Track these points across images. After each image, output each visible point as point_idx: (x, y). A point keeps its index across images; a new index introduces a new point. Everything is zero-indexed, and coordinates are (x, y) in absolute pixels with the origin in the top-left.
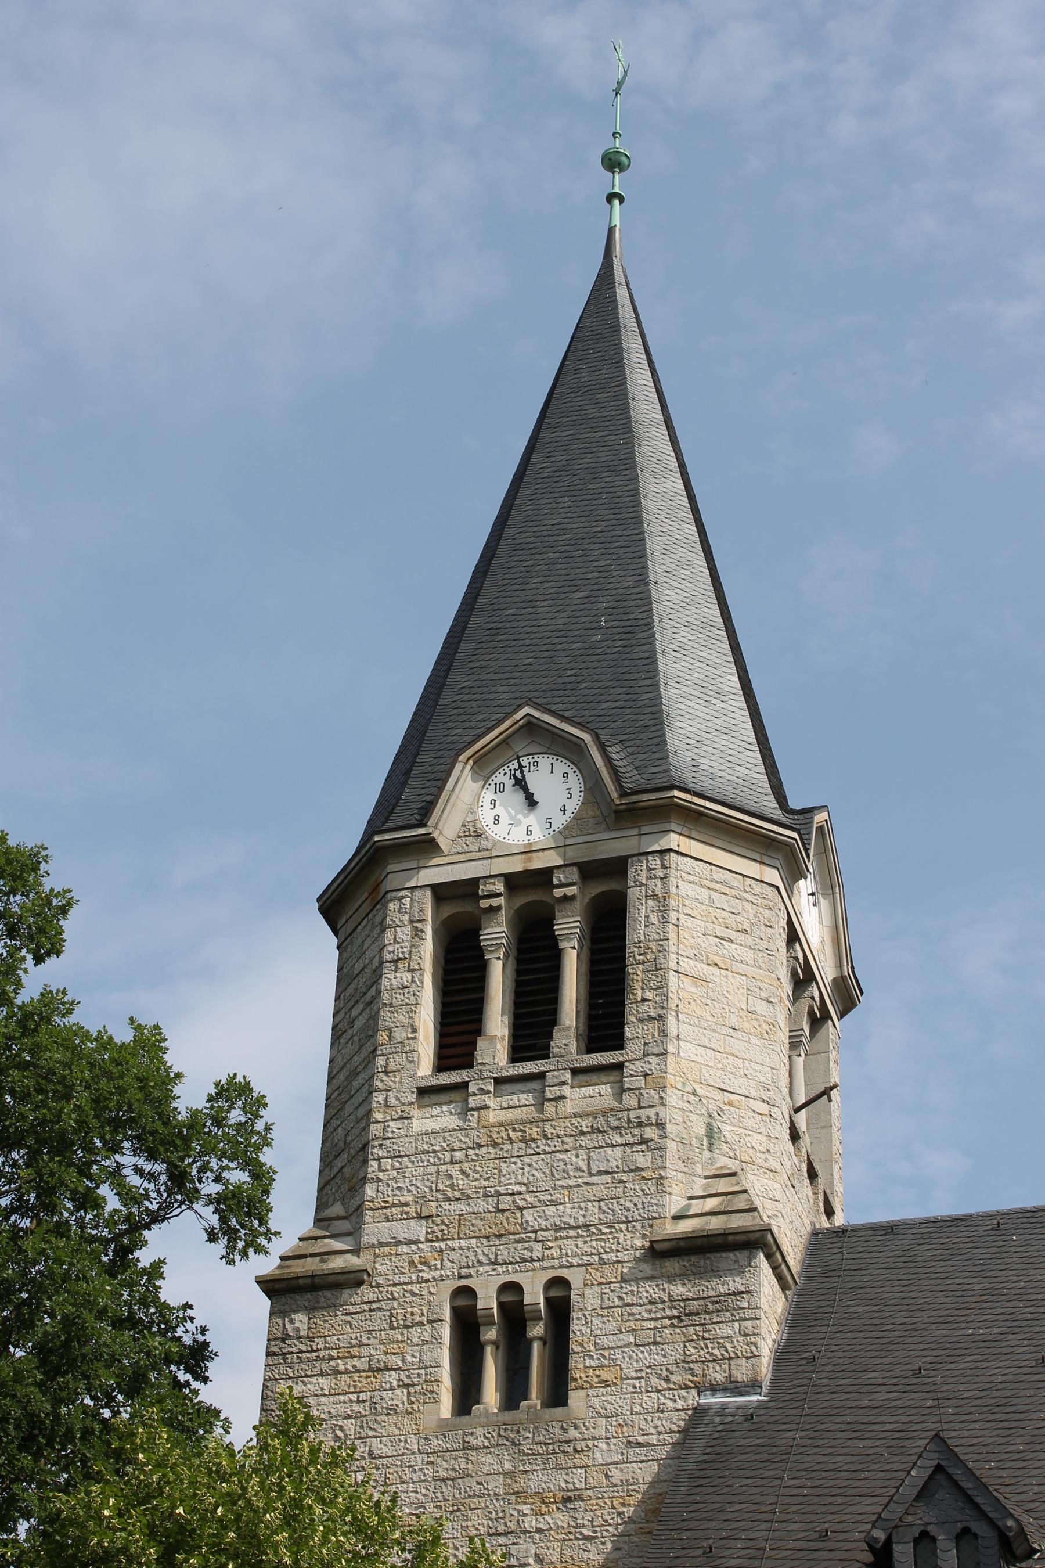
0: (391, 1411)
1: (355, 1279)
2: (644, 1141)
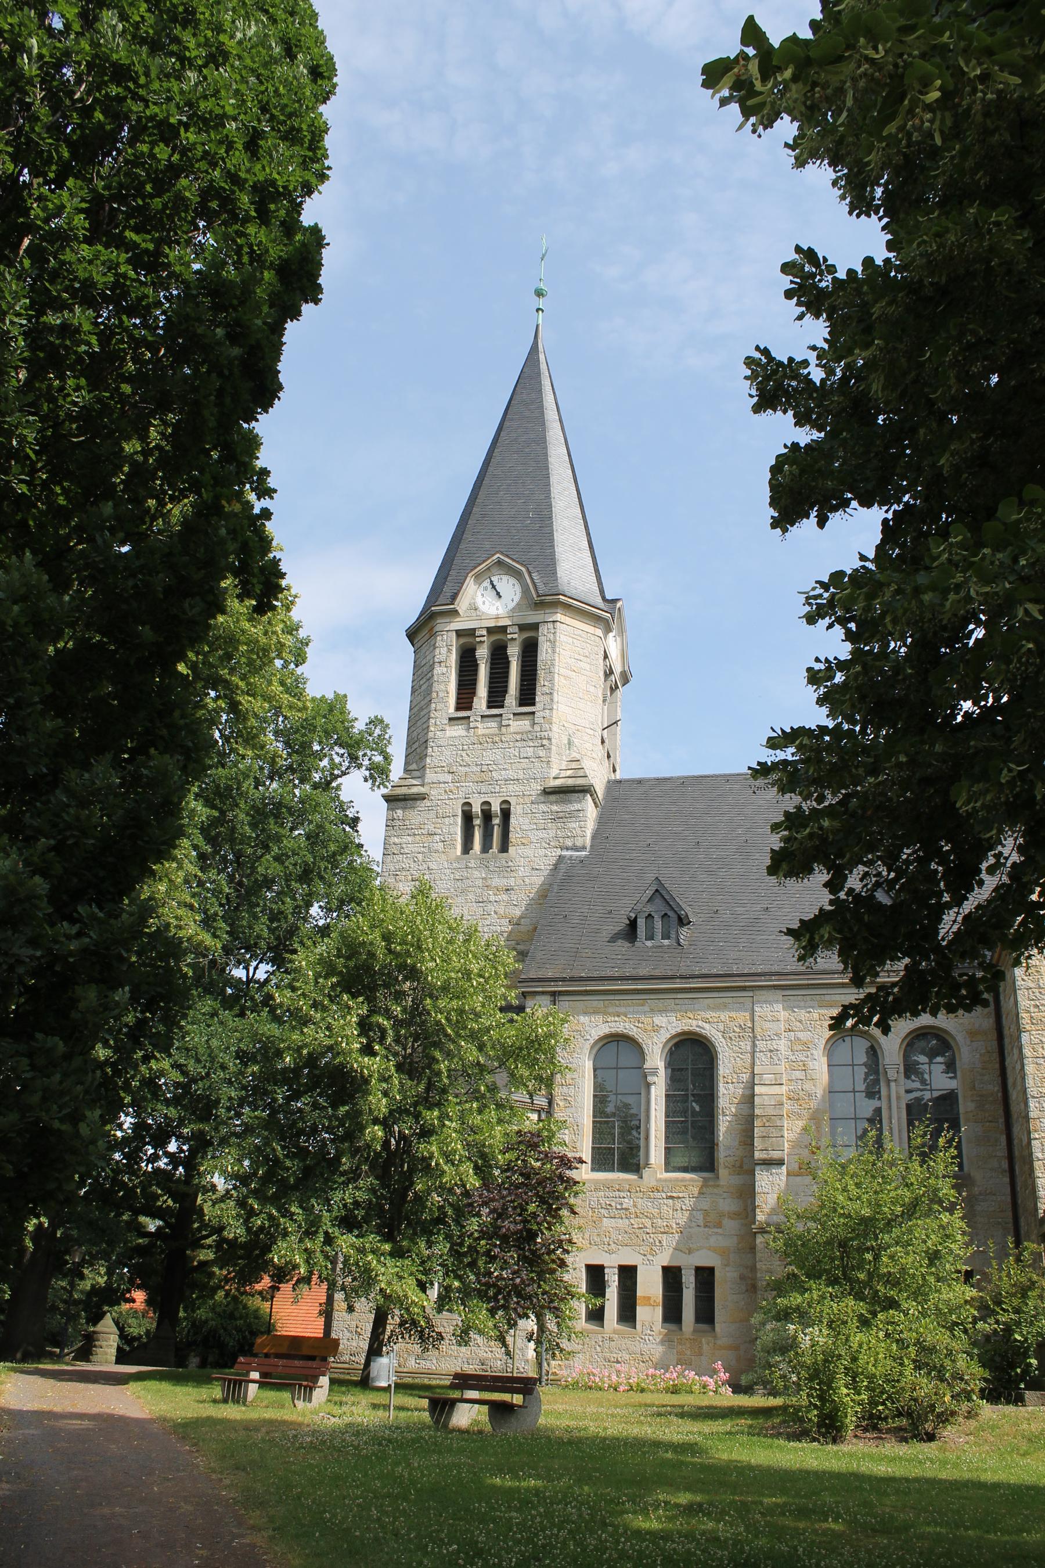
0: (436, 851)
1: (422, 797)
2: (543, 746)
